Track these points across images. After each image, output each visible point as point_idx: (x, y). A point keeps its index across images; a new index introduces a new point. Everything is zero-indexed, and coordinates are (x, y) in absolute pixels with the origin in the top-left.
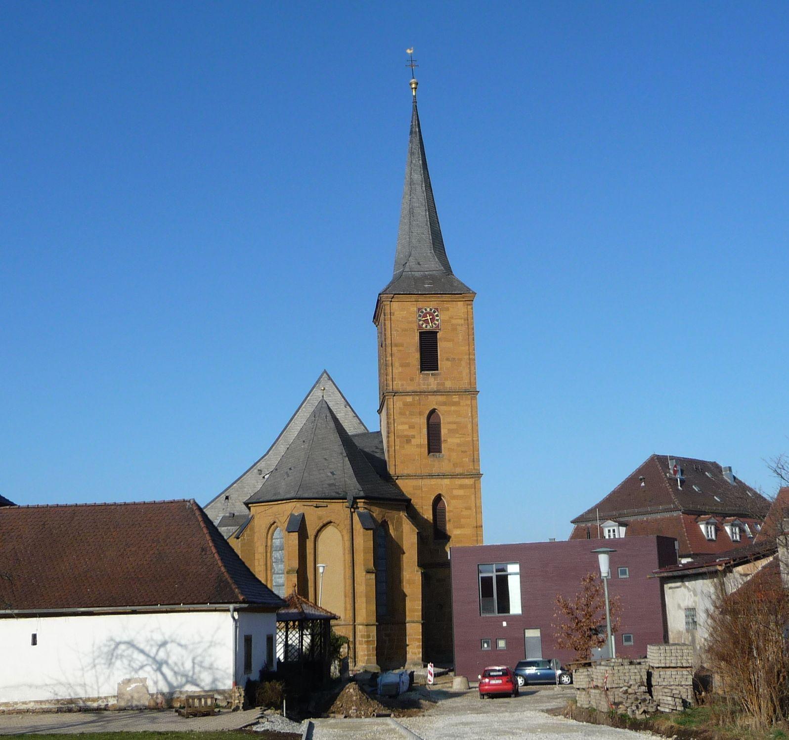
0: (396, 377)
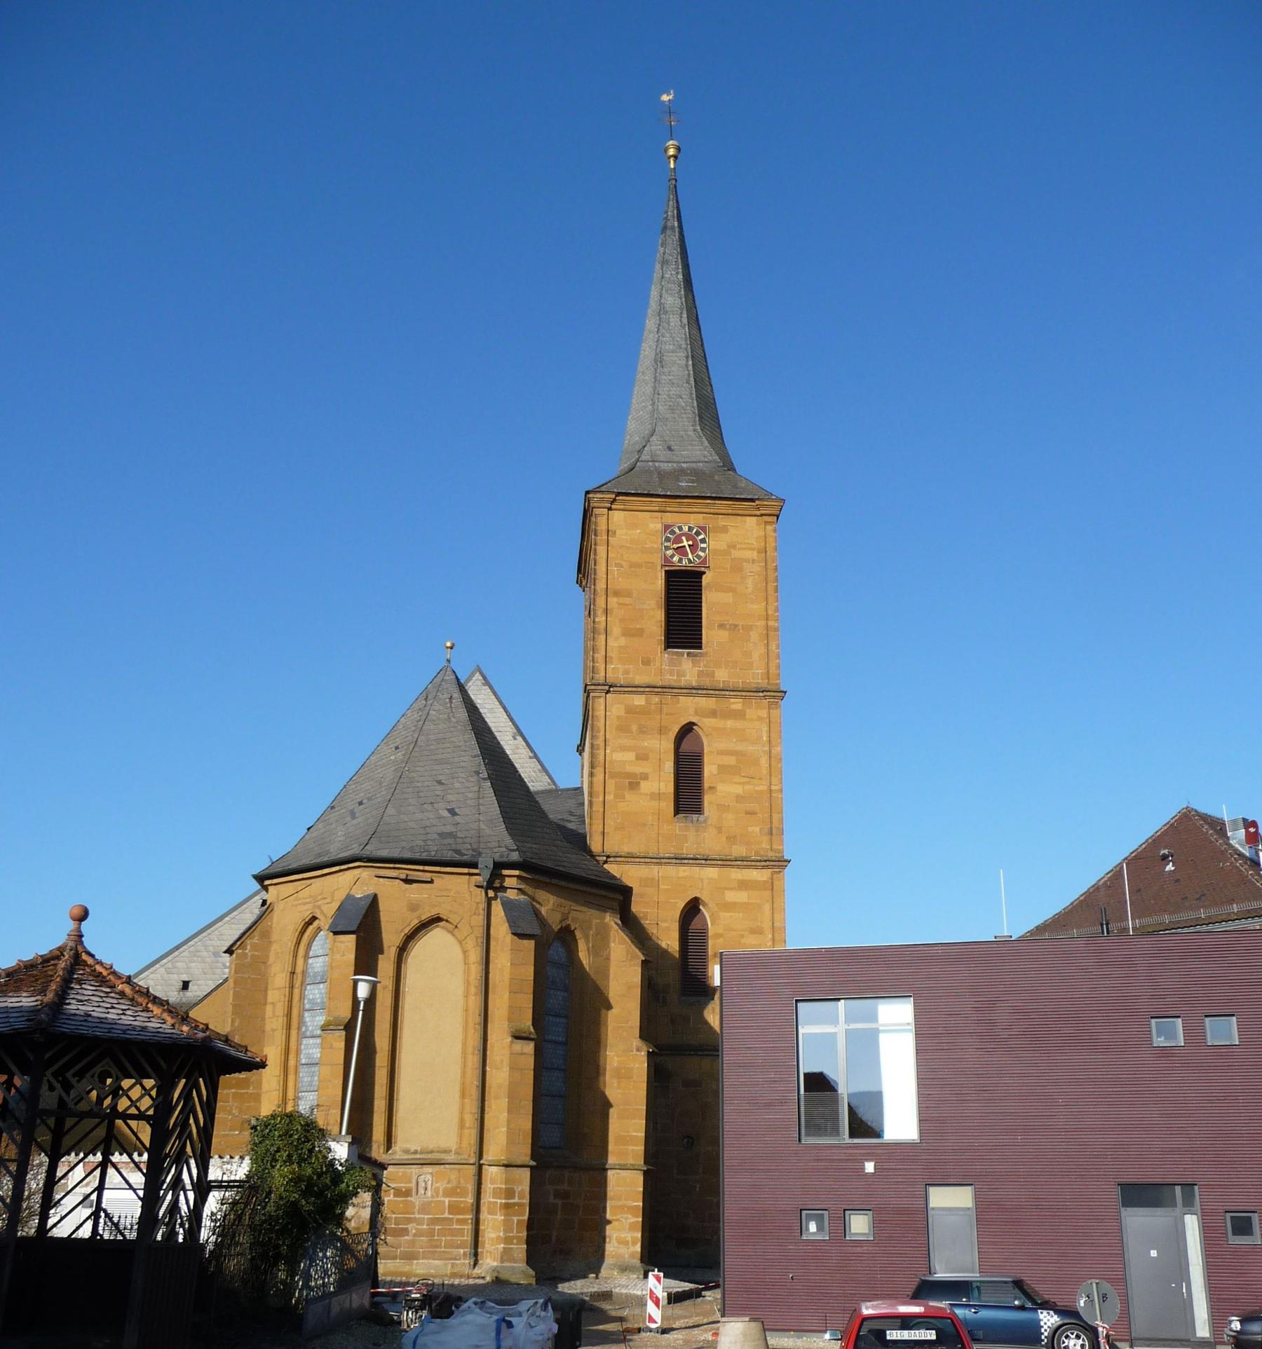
0: (613, 656)
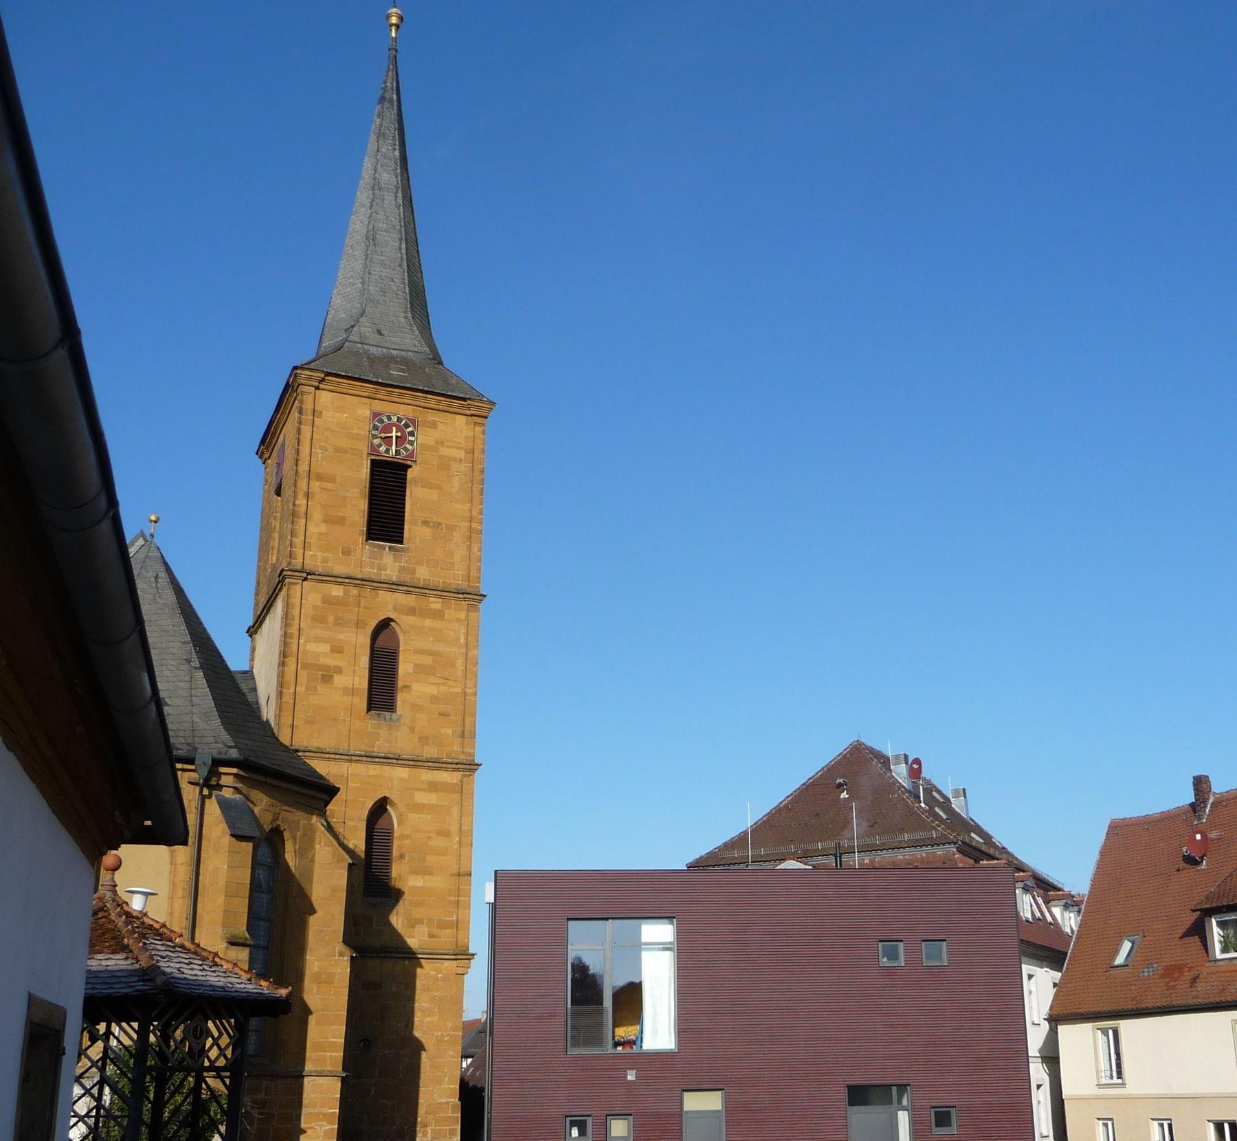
0: (312, 542)
